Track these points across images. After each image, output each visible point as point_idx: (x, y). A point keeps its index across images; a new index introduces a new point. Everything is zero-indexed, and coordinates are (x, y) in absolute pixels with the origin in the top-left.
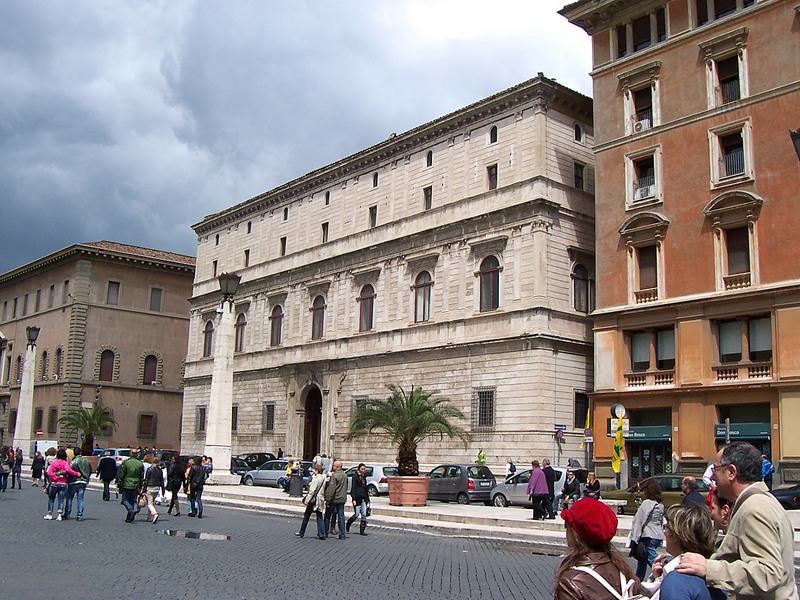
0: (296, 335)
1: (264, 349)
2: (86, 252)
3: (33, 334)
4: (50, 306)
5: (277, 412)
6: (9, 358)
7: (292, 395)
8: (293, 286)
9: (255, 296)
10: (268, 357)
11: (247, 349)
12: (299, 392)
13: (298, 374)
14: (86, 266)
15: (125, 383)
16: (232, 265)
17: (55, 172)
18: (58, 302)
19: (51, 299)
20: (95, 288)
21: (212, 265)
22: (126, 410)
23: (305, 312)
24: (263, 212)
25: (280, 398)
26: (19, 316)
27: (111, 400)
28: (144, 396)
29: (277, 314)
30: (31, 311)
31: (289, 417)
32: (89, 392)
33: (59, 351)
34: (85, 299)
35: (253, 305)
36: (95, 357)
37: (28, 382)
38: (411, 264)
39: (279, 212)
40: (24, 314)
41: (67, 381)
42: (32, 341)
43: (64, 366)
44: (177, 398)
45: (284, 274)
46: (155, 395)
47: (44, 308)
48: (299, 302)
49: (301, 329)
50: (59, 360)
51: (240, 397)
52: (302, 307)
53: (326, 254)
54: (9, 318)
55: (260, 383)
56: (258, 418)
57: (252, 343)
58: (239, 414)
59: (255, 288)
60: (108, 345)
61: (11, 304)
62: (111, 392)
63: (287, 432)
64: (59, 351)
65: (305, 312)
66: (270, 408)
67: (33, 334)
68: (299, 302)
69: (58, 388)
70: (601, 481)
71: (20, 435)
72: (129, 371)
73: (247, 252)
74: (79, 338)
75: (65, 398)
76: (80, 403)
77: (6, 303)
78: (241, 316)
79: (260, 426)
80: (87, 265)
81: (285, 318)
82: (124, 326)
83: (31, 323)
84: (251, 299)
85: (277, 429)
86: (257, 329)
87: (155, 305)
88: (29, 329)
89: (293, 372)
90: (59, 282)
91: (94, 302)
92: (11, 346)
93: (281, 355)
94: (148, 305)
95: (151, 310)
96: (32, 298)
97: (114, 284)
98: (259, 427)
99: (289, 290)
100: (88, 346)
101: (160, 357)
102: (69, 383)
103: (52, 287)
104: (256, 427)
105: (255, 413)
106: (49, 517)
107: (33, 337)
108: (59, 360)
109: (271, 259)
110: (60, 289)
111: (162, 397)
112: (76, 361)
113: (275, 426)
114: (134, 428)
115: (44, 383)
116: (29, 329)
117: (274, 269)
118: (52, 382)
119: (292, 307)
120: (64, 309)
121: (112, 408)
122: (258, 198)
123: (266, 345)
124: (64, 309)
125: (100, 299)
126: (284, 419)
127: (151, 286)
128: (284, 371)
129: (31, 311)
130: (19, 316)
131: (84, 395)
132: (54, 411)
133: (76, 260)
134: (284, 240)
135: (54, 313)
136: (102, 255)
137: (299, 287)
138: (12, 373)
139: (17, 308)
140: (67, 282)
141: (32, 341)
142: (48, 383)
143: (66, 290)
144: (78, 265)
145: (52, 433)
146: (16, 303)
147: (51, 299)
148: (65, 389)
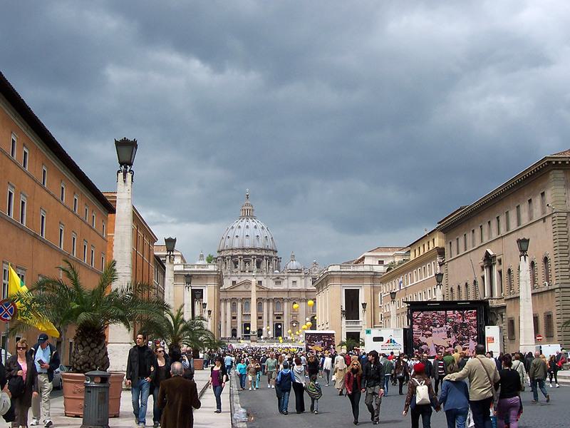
2: (557, 162)
3: (524, 246)
6: (500, 272)
17: (504, 101)
18: (537, 214)
19: (531, 212)
26: (503, 232)
30: (513, 226)
33: (546, 260)
37: (525, 291)
40: (508, 230)
41: (557, 286)
42: (523, 252)
43: (553, 273)
47: (525, 221)
50: (547, 268)
54: (494, 236)
60: (368, 335)
61: (494, 223)
64: (546, 260)
67: (523, 245)
69: (550, 294)
71: (525, 341)
75: (558, 303)
77: (489, 222)
80: (559, 174)
83: (524, 234)
88: (519, 241)
90: (535, 195)
92: (500, 261)
96: (513, 214)
102: (560, 288)
103: (530, 201)
106: (269, 387)
107: (524, 248)
108: (547, 268)
110: (537, 201)
112: (563, 266)
115: (512, 296)
116: (519, 241)
118: (543, 290)
120: (544, 219)
124: (544, 219)
129: (513, 226)
130: (503, 232)
132: (548, 317)
133: (550, 171)
135: (535, 225)
139: (483, 233)
140: (543, 194)
141: (523, 252)
143: (543, 201)
144: (552, 175)
145: (550, 337)
146: (499, 221)
147: (531, 212)
148: (556, 295)
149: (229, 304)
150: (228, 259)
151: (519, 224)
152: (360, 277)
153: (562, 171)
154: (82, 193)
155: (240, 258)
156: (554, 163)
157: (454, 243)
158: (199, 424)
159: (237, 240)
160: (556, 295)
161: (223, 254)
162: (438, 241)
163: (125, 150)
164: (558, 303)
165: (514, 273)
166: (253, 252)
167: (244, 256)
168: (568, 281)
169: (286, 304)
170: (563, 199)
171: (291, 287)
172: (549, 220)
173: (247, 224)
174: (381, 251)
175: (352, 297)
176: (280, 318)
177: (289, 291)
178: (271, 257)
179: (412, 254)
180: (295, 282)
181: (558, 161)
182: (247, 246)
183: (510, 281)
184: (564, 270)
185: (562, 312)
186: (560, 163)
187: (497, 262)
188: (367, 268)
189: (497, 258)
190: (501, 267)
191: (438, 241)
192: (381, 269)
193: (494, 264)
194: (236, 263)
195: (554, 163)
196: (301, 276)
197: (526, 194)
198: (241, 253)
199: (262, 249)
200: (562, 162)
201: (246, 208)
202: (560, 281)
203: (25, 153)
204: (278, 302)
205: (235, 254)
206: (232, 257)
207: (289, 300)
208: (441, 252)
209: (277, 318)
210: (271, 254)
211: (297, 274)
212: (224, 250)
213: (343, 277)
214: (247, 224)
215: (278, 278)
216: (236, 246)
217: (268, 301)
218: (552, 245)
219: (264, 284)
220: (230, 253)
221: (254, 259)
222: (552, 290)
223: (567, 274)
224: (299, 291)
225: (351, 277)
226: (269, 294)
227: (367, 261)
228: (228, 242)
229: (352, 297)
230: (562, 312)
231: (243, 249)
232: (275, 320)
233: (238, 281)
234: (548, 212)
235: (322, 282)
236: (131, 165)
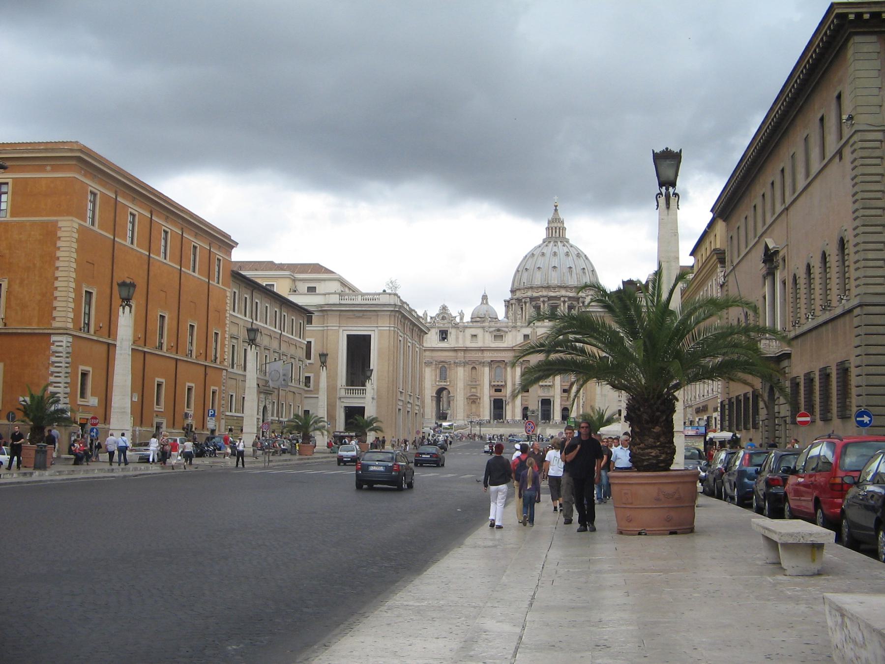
41: (855, 302)
69: (847, 318)
75: (857, 341)
102: (861, 305)
112: (871, 255)
150: (525, 303)
153: (873, 38)
155: (544, 302)
156: (852, 17)
158: (641, 484)
159: (525, 275)
161: (519, 295)
163: (666, 164)
168: (880, 289)
170: (875, 100)
171: (469, 344)
173: (555, 249)
175: (359, 348)
176: (500, 391)
177: (466, 350)
180: (475, 336)
181: (861, 14)
184: (871, 263)
185: (866, 360)
186: (866, 16)
187: (781, 261)
189: (781, 254)
193: (776, 268)
195: (852, 17)
196: (483, 328)
197: (816, 107)
198: (545, 293)
199: (560, 287)
201: (556, 225)
205: (535, 295)
206: (532, 299)
207: (465, 364)
209: (496, 391)
211: (479, 324)
212: (519, 289)
214: (555, 249)
215: (499, 330)
216: (537, 282)
218: (851, 207)
220: (529, 294)
221: (564, 302)
222: (850, 311)
223: (880, 272)
224: (482, 350)
225: (789, 299)
226: (468, 355)
229: (359, 348)
231: (548, 288)
232: (493, 393)
236: (674, 185)
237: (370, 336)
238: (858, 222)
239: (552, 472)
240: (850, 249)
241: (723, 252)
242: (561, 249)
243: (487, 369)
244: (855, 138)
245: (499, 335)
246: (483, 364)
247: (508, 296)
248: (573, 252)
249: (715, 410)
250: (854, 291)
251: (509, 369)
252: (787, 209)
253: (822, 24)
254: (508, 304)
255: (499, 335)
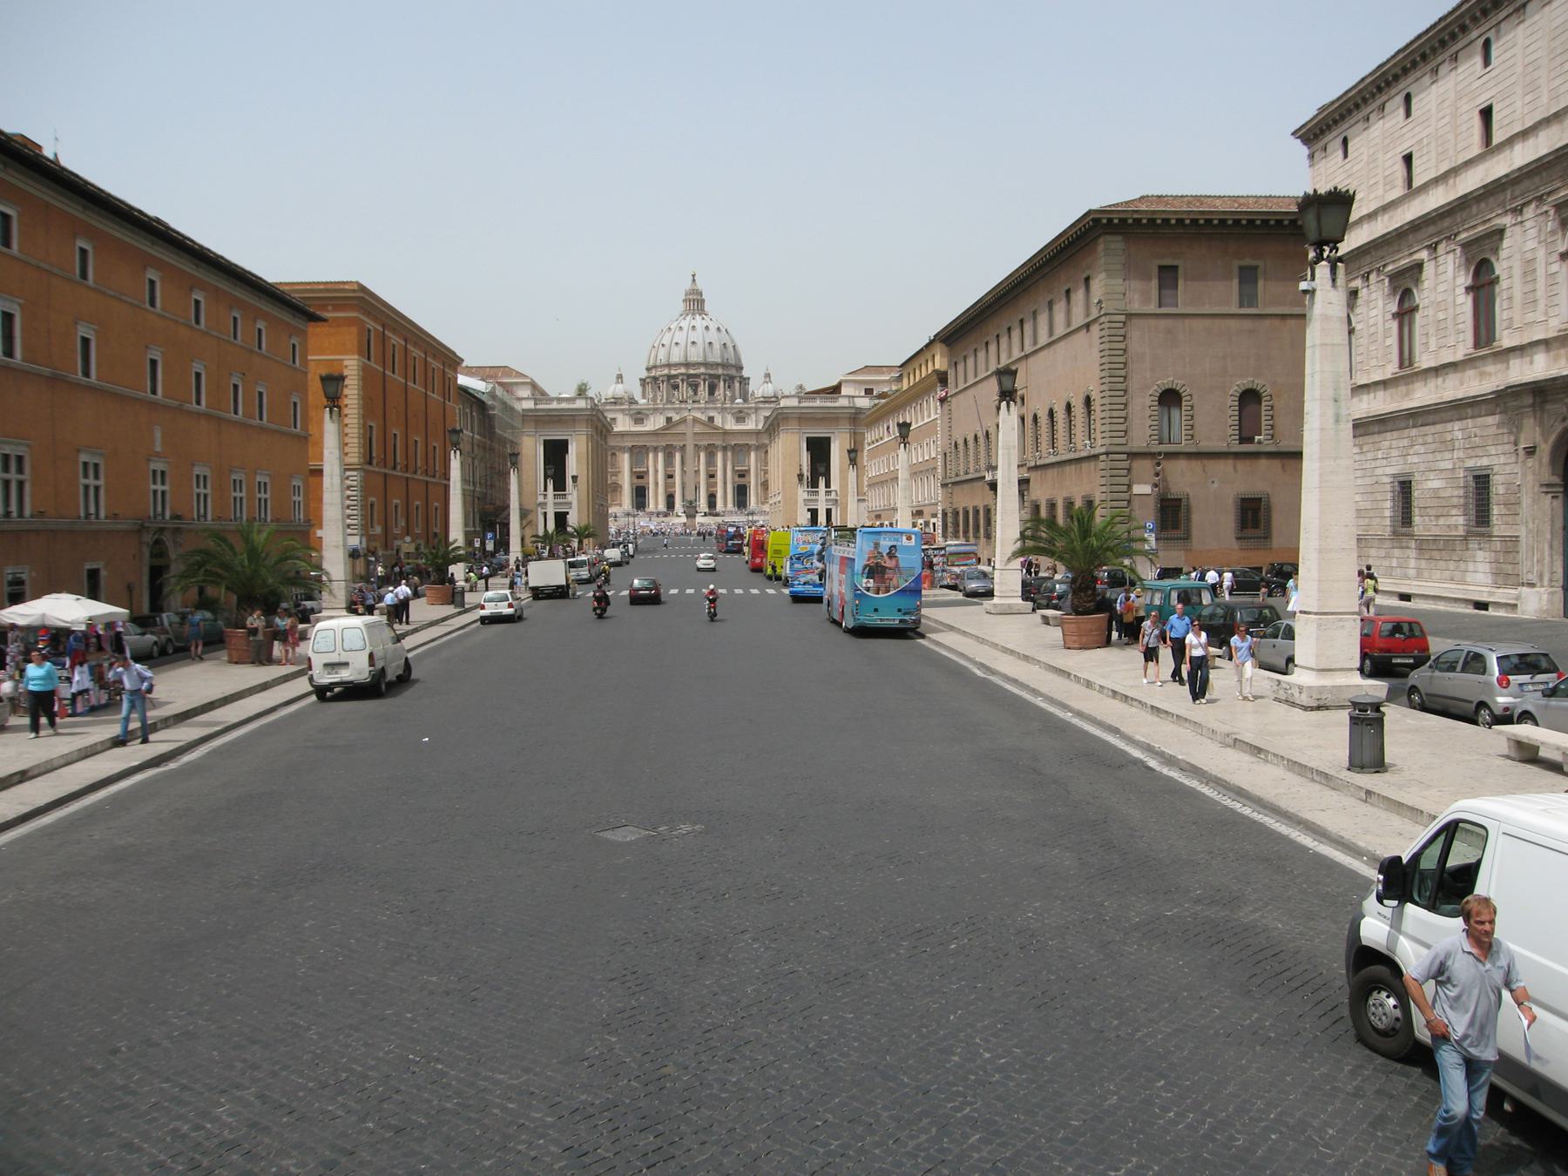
0: (1530, 317)
1: (1459, 357)
2: (1110, 220)
4: (1069, 324)
5: (1498, 488)
7: (1531, 451)
8: (1518, 211)
9: (1433, 248)
10: (1470, 373)
11: (1424, 361)
12: (1545, 449)
13: (1544, 402)
14: (1113, 246)
15: (1206, 445)
16: (1380, 192)
18: (1079, 319)
20: (1136, 284)
21: (1399, 169)
22: (1213, 494)
23: (1548, 264)
24: (1433, 64)
25: (1502, 459)
26: (1028, 349)
27: (1182, 478)
28: (1242, 465)
29: (1483, 279)
31: (1526, 501)
32: (1143, 467)
33: (1088, 401)
34: (1120, 305)
35: (1429, 270)
36: (1148, 403)
38: (1466, 246)
39: (1470, 56)
41: (1103, 450)
42: (1008, 395)
43: (1098, 426)
44: (1291, 463)
45: (1415, 226)
46: (1263, 462)
47: (1060, 330)
48: (1531, 244)
49: (1541, 306)
51: (1416, 459)
52: (1541, 254)
53: (1499, 167)
55: (1456, 430)
56: (1455, 501)
57: (1433, 347)
58: (1415, 494)
59: (1432, 229)
62: (1182, 464)
63: (1522, 532)
64: (1088, 401)
65: (1548, 264)
66: (1482, 482)
68: (1531, 244)
69: (1092, 464)
70: (410, 655)
72: (1213, 422)
73: (1408, 159)
74: (1118, 373)
75: (1103, 481)
76: (1129, 486)
78: (1406, 294)
79: (1461, 520)
80: (1115, 243)
81: (1504, 284)
82: (1198, 347)
84: (1424, 255)
85: (1499, 526)
86: (1441, 316)
87: (1247, 298)
89: (1529, 400)
91: (1136, 307)
92: (1023, 399)
93: (1499, 366)
94: (1235, 298)
95: (1241, 306)
97: (1168, 276)
98: (1458, 521)
99: (1507, 220)
100: (1134, 384)
101: (1266, 391)
102: (1107, 454)
104: (1452, 521)
105: (1447, 493)
109: (1460, 161)
110: (1079, 296)
111: (1276, 463)
113: (1495, 519)
114: (1228, 522)
117: (1470, 182)
118: (1084, 454)
119: (1518, 256)
120: (1087, 326)
121: (1188, 490)
122: (1419, 37)
123: (1463, 347)
124: (1087, 326)
125: (1146, 301)
126: (1512, 505)
127: (1237, 263)
128: (1506, 400)
131: (1134, 472)
134: (1486, 114)
136: (1140, 220)
137: (1529, 212)
138: (971, 458)
142: (1077, 456)
148: (1102, 465)
149: (660, 455)
151: (1051, 333)
152: (831, 418)
153: (1120, 238)
154: (1167, 204)
157: (960, 367)
160: (1102, 465)
162: (939, 362)
164: (1103, 481)
165: (992, 437)
166: (702, 370)
167: (689, 376)
169: (753, 454)
170: (1121, 289)
172: (1095, 328)
174: (870, 373)
178: (732, 378)
179: (905, 380)
182: (693, 358)
183: (988, 449)
185: (1110, 496)
188: (842, 402)
190: (1024, 410)
191: (939, 362)
192: (864, 403)
194: (676, 387)
199: (718, 365)
200: (1121, 220)
202: (1107, 441)
203: (83, 252)
204: (740, 450)
206: (670, 377)
208: (942, 378)
210: (733, 372)
213: (803, 418)
217: (725, 449)
218: (1098, 374)
219: (718, 421)
220: (666, 371)
227: (845, 391)
228: (662, 356)
230: (1110, 496)
233: (676, 417)
234: (1094, 313)
235: (774, 425)
237: (546, 442)
238: (1104, 387)
239: (1383, 694)
240: (1096, 406)
241: (946, 373)
242: (699, 322)
243: (626, 456)
244: (1103, 319)
245: (639, 417)
246: (622, 449)
247: (644, 374)
248: (713, 327)
249: (934, 516)
250: (1100, 442)
251: (651, 456)
252: (1026, 357)
253: (1073, 225)
254: (643, 382)
255: (639, 417)
